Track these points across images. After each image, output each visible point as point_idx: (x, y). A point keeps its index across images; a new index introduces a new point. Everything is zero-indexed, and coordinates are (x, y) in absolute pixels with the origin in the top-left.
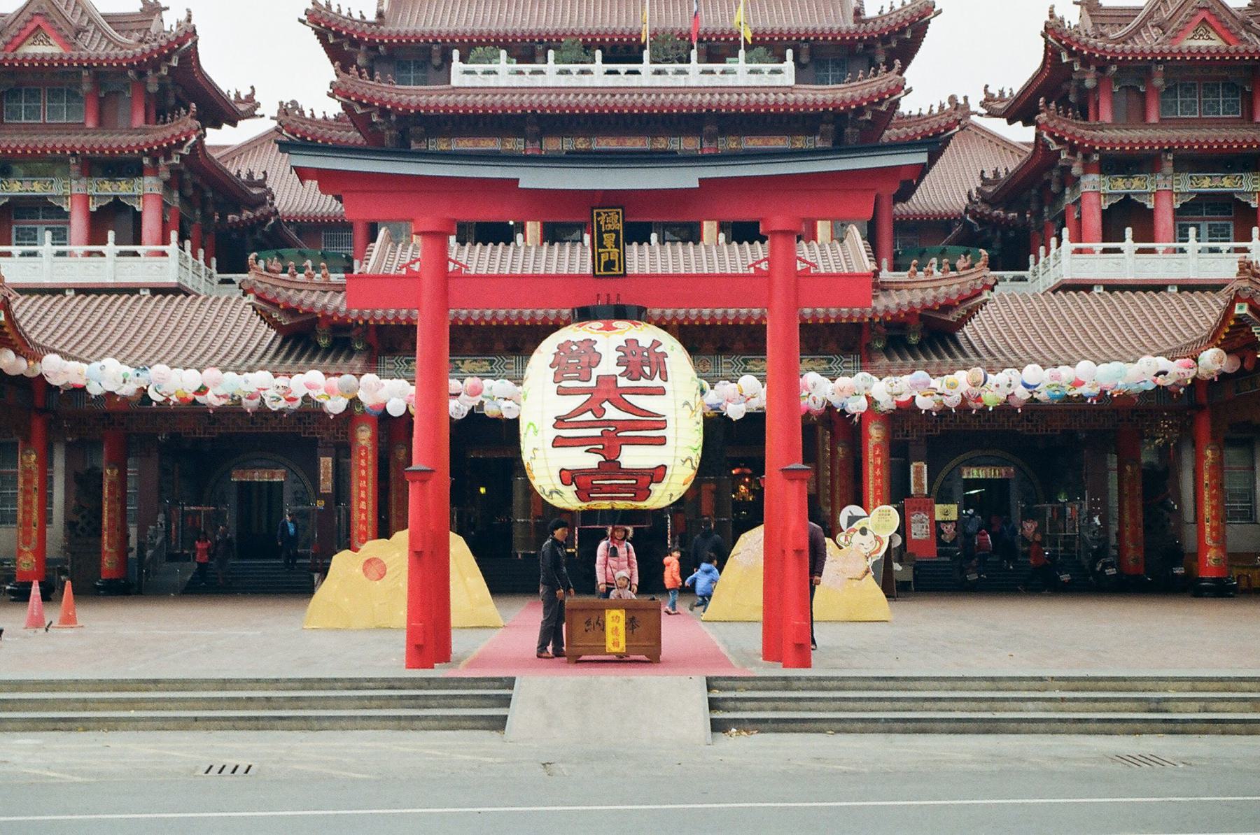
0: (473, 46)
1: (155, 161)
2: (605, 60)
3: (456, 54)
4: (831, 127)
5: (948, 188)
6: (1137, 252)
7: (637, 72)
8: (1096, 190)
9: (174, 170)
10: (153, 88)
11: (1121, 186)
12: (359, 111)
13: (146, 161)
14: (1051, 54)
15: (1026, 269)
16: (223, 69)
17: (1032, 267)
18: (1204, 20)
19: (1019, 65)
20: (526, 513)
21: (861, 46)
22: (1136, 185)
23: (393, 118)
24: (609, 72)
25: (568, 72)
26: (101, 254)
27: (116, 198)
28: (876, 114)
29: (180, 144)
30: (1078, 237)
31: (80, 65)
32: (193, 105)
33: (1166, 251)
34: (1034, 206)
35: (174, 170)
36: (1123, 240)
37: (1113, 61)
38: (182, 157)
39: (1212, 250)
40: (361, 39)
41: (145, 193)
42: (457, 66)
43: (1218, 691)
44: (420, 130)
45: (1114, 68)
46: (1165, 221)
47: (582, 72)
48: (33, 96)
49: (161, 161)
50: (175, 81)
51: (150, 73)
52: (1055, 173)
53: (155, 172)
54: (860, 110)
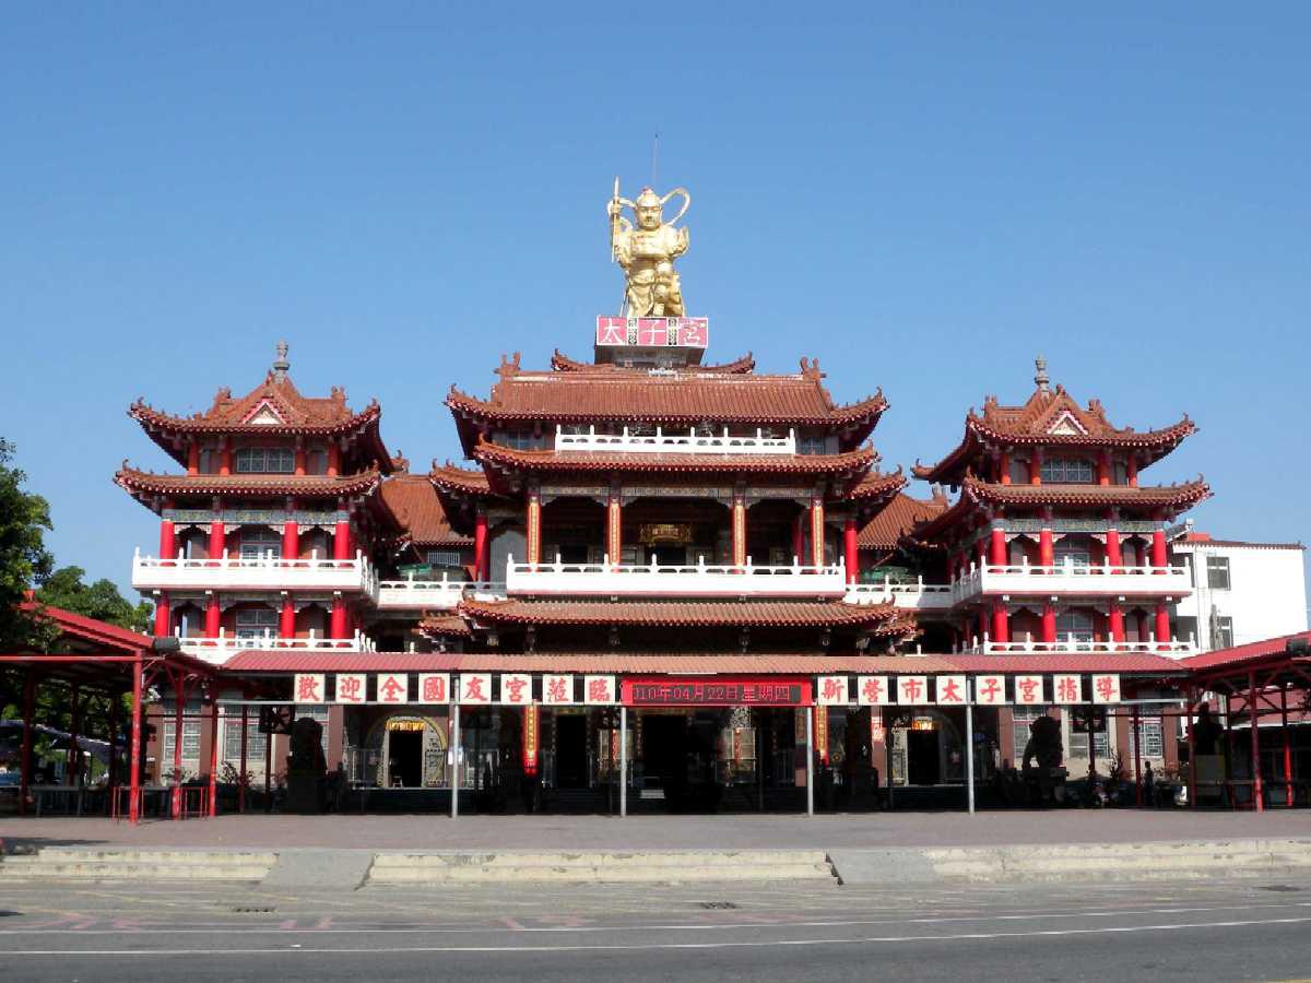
0: (575, 423)
1: (346, 500)
2: (664, 434)
3: (559, 428)
4: (824, 483)
5: (885, 530)
6: (564, 571)
7: (585, 441)
8: (1004, 530)
9: (358, 507)
10: (345, 448)
11: (1131, 527)
12: (494, 466)
13: (341, 499)
14: (970, 436)
15: (949, 582)
16: (392, 440)
17: (953, 582)
18: (1067, 419)
19: (945, 443)
20: (595, 778)
21: (834, 428)
22: (197, 517)
23: (517, 472)
24: (667, 442)
25: (671, 442)
26: (218, 565)
27: (193, 525)
28: (855, 474)
29: (367, 488)
30: (991, 561)
31: (297, 432)
32: (376, 461)
33: (206, 565)
34: (952, 540)
35: (358, 507)
36: (792, 564)
37: (1012, 443)
38: (367, 497)
39: (194, 565)
40: (486, 416)
41: (336, 522)
42: (559, 437)
43: (840, 921)
44: (535, 480)
45: (1011, 448)
46: (1047, 552)
47: (681, 442)
48: (258, 454)
49: (351, 499)
50: (359, 446)
51: (344, 438)
52: (971, 517)
53: (346, 507)
54: (845, 472)
